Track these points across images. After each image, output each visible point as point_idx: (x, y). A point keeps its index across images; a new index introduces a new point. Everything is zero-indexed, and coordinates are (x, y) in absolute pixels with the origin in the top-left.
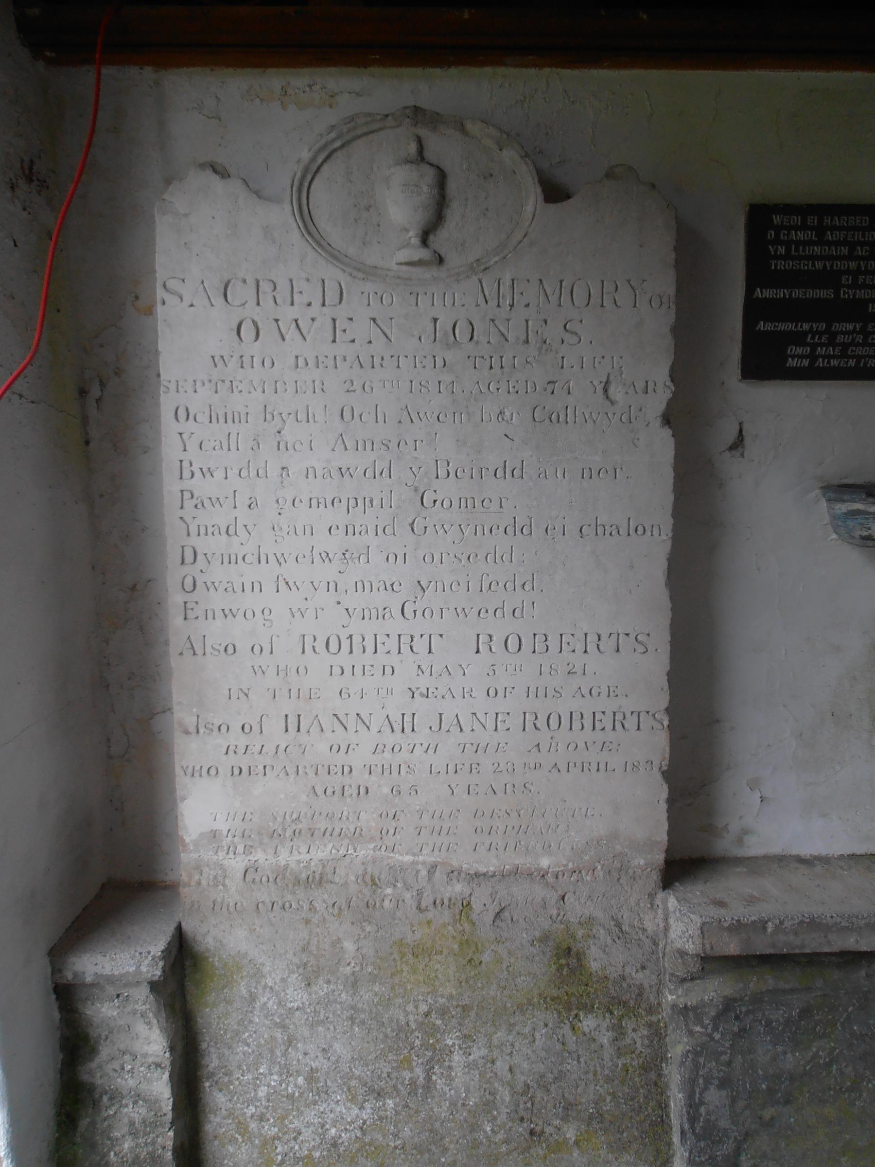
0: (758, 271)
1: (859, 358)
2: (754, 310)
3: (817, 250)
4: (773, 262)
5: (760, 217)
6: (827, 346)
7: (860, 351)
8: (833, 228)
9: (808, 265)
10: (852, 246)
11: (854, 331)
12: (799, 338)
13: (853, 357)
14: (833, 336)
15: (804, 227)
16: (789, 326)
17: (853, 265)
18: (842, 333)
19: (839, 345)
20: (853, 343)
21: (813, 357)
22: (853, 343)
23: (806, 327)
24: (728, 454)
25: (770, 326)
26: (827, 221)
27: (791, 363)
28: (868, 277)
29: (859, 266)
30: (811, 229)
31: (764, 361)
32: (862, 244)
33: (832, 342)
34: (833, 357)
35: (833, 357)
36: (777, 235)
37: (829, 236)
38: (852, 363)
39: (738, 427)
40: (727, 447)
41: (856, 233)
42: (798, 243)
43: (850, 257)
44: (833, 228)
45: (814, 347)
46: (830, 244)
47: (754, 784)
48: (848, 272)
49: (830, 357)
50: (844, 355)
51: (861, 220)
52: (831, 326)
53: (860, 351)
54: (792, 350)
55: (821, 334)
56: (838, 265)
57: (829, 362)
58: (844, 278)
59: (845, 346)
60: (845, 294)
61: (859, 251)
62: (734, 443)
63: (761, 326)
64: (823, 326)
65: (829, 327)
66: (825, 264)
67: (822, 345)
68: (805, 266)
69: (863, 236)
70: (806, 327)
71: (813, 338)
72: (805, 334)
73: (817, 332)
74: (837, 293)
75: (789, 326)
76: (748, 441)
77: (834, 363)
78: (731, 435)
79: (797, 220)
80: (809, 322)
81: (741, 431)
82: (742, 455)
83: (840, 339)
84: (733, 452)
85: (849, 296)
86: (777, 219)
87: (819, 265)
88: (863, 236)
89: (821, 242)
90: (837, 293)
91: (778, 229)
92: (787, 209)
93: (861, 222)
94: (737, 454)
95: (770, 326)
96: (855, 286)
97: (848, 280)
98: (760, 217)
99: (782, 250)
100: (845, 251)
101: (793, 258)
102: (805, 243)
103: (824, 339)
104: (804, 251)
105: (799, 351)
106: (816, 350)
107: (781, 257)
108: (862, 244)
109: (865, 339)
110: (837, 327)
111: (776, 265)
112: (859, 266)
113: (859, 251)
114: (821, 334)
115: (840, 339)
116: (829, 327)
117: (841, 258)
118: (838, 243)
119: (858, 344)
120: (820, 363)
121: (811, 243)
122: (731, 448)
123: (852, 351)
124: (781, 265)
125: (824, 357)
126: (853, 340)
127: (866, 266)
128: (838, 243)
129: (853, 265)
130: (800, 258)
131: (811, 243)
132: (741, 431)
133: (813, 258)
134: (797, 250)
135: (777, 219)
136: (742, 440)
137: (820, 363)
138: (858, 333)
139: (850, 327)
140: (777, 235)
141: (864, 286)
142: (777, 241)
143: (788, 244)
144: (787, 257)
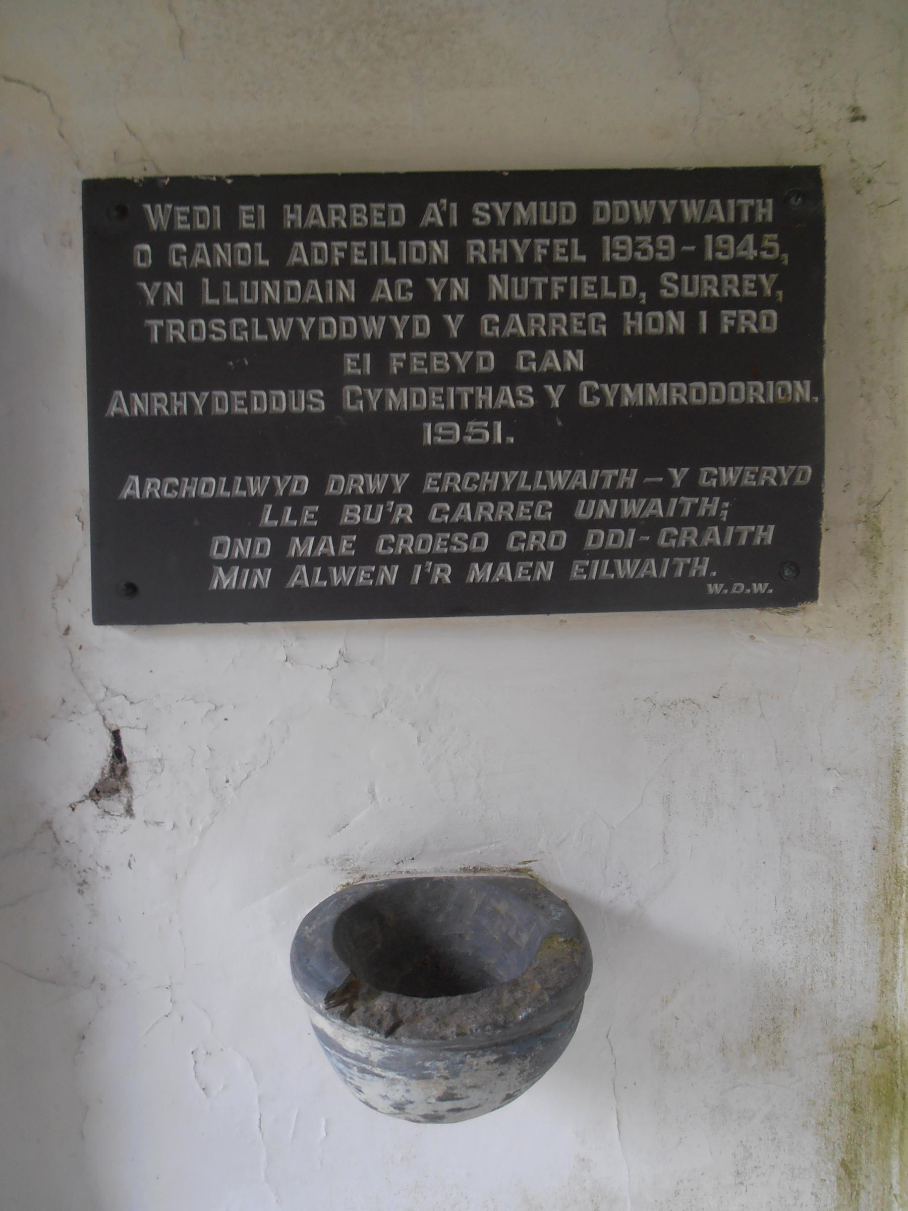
0: (118, 348)
1: (406, 562)
2: (115, 448)
3: (270, 291)
4: (155, 324)
5: (114, 211)
6: (317, 533)
7: (407, 544)
8: (311, 235)
9: (249, 329)
10: (365, 280)
11: (389, 493)
12: (240, 517)
13: (389, 561)
14: (330, 511)
15: (230, 232)
16: (209, 487)
17: (373, 327)
18: (354, 498)
19: (349, 530)
20: (386, 525)
21: (281, 564)
22: (386, 525)
23: (256, 487)
24: (90, 808)
25: (155, 488)
26: (292, 216)
27: (223, 580)
28: (415, 355)
29: (389, 328)
30: (250, 236)
31: (151, 574)
32: (393, 274)
33: (329, 524)
34: (339, 561)
35: (339, 561)
36: (161, 254)
37: (298, 255)
38: (389, 575)
39: (109, 742)
40: (87, 790)
41: (374, 244)
42: (218, 275)
43: (363, 306)
44: (311, 235)
45: (281, 537)
46: (303, 273)
47: (478, 1001)
48: (360, 344)
49: (326, 562)
50: (365, 553)
51: (386, 213)
52: (325, 485)
53: (407, 544)
54: (223, 546)
55: (298, 504)
56: (332, 328)
57: (325, 576)
58: (350, 360)
59: (366, 535)
60: (353, 398)
61: (383, 291)
62: (103, 782)
63: (132, 488)
64: (302, 483)
65: (319, 484)
66: (296, 326)
67: (303, 533)
68: (239, 330)
69: (394, 252)
70: (256, 487)
71: (277, 514)
72: (256, 504)
73: (287, 499)
74: (333, 398)
75: (209, 487)
76: (138, 776)
77: (341, 577)
78: (94, 759)
79: (208, 216)
80: (381, 471)
81: (118, 754)
82: (129, 811)
83: (351, 515)
84: (105, 803)
85: (367, 404)
86: (156, 217)
87: (280, 330)
88: (394, 252)
89: (279, 270)
90: (333, 398)
91: (161, 241)
92: (185, 189)
93: (386, 217)
94: (116, 805)
95: (155, 488)
96: (380, 377)
97: (360, 364)
98: (114, 211)
99: (174, 293)
100: (346, 291)
101: (208, 313)
102: (237, 275)
103: (308, 515)
104: (235, 293)
105: (242, 548)
106: (287, 545)
107: (173, 311)
108: (393, 274)
109: (421, 514)
110: (338, 484)
111: (162, 331)
112: (389, 328)
113: (383, 291)
114: (298, 504)
115: (351, 515)
116: (319, 484)
117: (338, 309)
118: (325, 273)
119: (402, 528)
120: (299, 578)
121: (254, 273)
122: (97, 793)
123: (386, 544)
124: (177, 331)
125: (311, 562)
126: (387, 516)
127: (408, 329)
128: (325, 273)
129: (373, 327)
130: (227, 312)
131: (254, 273)
132: (118, 754)
133: (264, 311)
134: (216, 292)
135: (156, 217)
136: (125, 771)
137: (299, 578)
138: (400, 499)
139: (376, 484)
140: (161, 254)
141: (406, 379)
142: (161, 270)
143: (191, 278)
144: (191, 308)
